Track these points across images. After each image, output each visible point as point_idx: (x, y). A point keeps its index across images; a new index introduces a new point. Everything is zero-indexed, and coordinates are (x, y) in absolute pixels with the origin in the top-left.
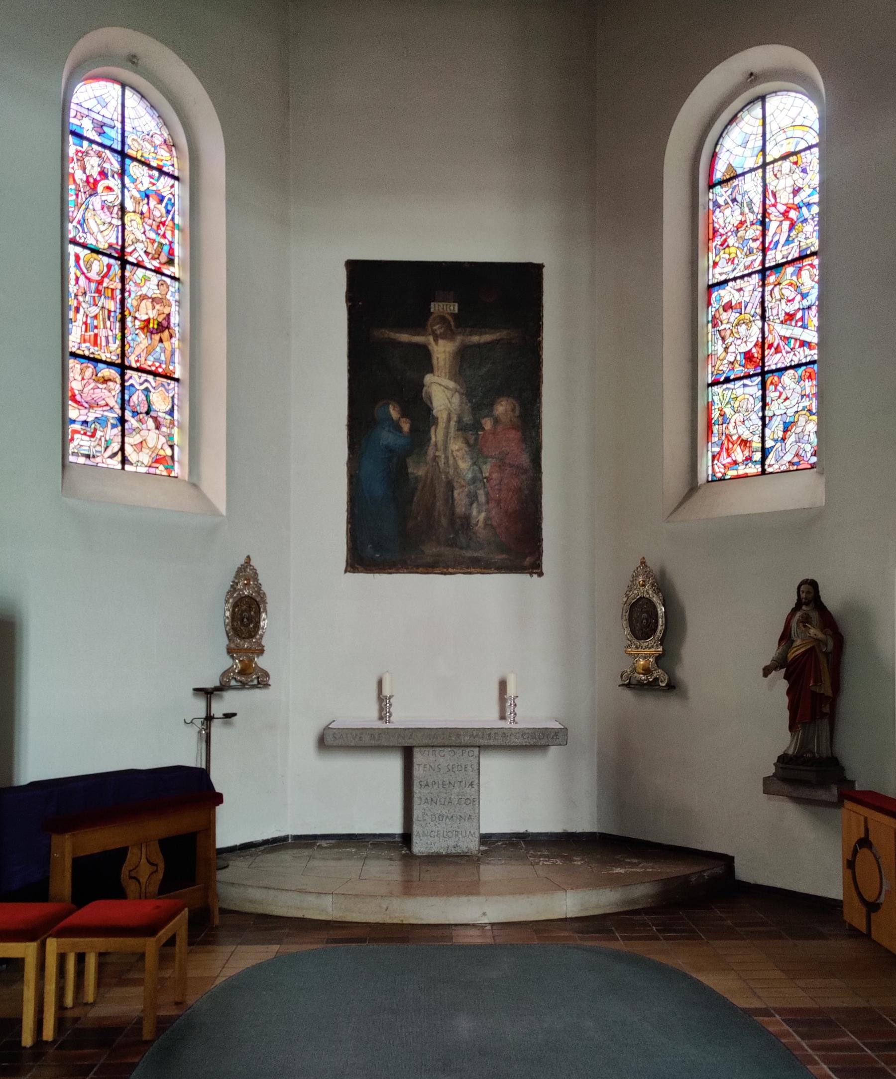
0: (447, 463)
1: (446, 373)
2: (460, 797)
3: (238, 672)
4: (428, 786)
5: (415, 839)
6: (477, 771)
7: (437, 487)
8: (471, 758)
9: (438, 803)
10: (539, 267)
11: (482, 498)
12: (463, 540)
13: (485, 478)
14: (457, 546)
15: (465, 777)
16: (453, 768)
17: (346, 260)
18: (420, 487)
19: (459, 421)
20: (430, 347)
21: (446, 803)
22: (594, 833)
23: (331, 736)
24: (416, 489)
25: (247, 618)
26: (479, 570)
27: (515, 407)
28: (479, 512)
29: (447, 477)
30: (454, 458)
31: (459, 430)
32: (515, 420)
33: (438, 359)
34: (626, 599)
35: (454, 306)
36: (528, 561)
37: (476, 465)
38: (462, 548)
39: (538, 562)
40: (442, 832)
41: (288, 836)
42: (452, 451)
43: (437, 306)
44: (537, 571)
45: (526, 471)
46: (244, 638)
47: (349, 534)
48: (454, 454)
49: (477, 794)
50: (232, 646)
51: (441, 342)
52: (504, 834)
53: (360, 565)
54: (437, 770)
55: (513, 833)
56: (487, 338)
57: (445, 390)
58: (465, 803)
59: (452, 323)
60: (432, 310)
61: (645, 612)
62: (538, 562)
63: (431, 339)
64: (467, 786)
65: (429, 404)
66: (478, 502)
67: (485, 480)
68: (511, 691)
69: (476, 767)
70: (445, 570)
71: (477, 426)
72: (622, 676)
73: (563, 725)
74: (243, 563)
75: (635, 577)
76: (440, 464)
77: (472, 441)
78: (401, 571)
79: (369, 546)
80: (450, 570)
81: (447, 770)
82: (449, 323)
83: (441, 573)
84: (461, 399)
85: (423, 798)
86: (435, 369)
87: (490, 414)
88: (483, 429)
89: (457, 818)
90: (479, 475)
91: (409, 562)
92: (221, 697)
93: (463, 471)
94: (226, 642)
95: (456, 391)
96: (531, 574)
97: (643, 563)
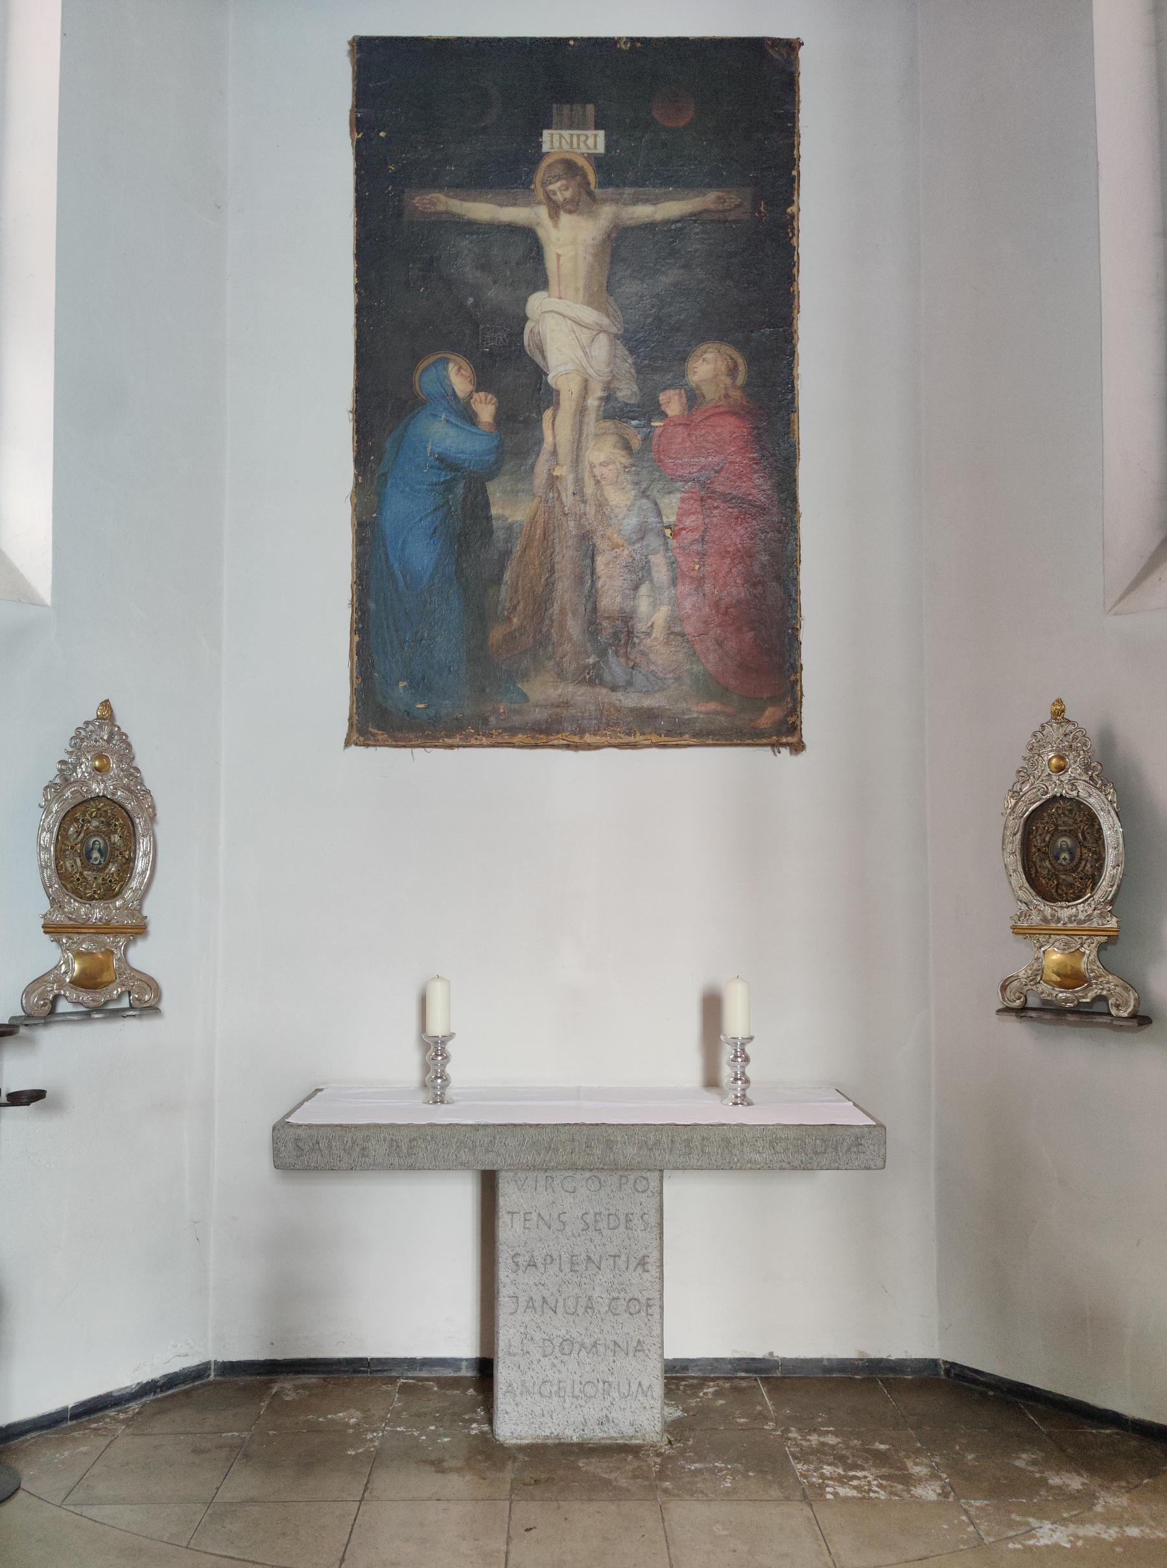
0: (579, 492)
1: (577, 290)
2: (615, 1295)
3: (70, 982)
4: (535, 1265)
5: (503, 1401)
6: (656, 1231)
7: (557, 549)
8: (642, 1198)
9: (560, 1310)
10: (791, 47)
11: (661, 573)
12: (616, 667)
13: (669, 527)
14: (602, 683)
15: (626, 1243)
16: (596, 1221)
17: (350, 38)
18: (517, 549)
19: (609, 397)
20: (541, 233)
21: (581, 1311)
22: (934, 1363)
23: (290, 1146)
24: (508, 553)
25: (100, 851)
26: (655, 739)
27: (736, 365)
28: (654, 605)
29: (580, 526)
30: (598, 482)
31: (608, 416)
32: (736, 394)
33: (559, 256)
34: (1013, 801)
35: (596, 136)
36: (770, 716)
37: (647, 497)
38: (614, 688)
39: (791, 720)
40: (569, 1382)
41: (209, 1363)
42: (592, 466)
43: (556, 137)
44: (790, 739)
45: (763, 510)
46: (92, 898)
47: (356, 658)
48: (597, 471)
49: (656, 1287)
50: (58, 918)
51: (565, 218)
52: (716, 1360)
53: (383, 729)
54: (556, 1225)
55: (740, 1360)
56: (671, 209)
57: (575, 327)
58: (627, 1310)
59: (592, 178)
60: (545, 148)
61: (1065, 833)
62: (791, 720)
63: (543, 211)
64: (632, 1267)
65: (538, 359)
66: (651, 581)
67: (668, 532)
68: (736, 1022)
69: (653, 1220)
70: (576, 739)
71: (648, 409)
72: (1004, 988)
73: (873, 1118)
74: (92, 716)
75: (1035, 750)
76: (563, 495)
77: (636, 443)
78: (473, 742)
79: (401, 685)
80: (588, 738)
81: (582, 1226)
82: (585, 176)
83: (568, 747)
84: (613, 346)
85: (523, 1300)
86: (553, 281)
87: (679, 380)
88: (663, 415)
89: (606, 1347)
90: (653, 519)
91: (492, 719)
92: (31, 1042)
93: (617, 510)
94: (45, 905)
95: (601, 330)
96: (776, 746)
97: (1058, 714)
